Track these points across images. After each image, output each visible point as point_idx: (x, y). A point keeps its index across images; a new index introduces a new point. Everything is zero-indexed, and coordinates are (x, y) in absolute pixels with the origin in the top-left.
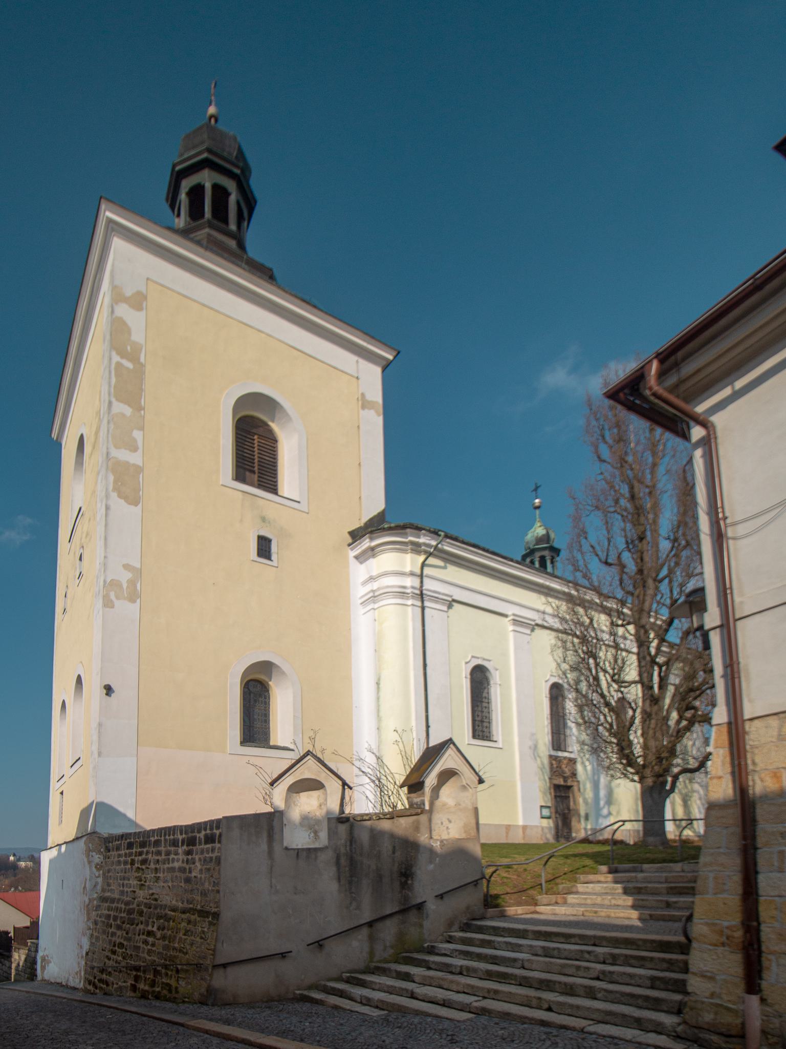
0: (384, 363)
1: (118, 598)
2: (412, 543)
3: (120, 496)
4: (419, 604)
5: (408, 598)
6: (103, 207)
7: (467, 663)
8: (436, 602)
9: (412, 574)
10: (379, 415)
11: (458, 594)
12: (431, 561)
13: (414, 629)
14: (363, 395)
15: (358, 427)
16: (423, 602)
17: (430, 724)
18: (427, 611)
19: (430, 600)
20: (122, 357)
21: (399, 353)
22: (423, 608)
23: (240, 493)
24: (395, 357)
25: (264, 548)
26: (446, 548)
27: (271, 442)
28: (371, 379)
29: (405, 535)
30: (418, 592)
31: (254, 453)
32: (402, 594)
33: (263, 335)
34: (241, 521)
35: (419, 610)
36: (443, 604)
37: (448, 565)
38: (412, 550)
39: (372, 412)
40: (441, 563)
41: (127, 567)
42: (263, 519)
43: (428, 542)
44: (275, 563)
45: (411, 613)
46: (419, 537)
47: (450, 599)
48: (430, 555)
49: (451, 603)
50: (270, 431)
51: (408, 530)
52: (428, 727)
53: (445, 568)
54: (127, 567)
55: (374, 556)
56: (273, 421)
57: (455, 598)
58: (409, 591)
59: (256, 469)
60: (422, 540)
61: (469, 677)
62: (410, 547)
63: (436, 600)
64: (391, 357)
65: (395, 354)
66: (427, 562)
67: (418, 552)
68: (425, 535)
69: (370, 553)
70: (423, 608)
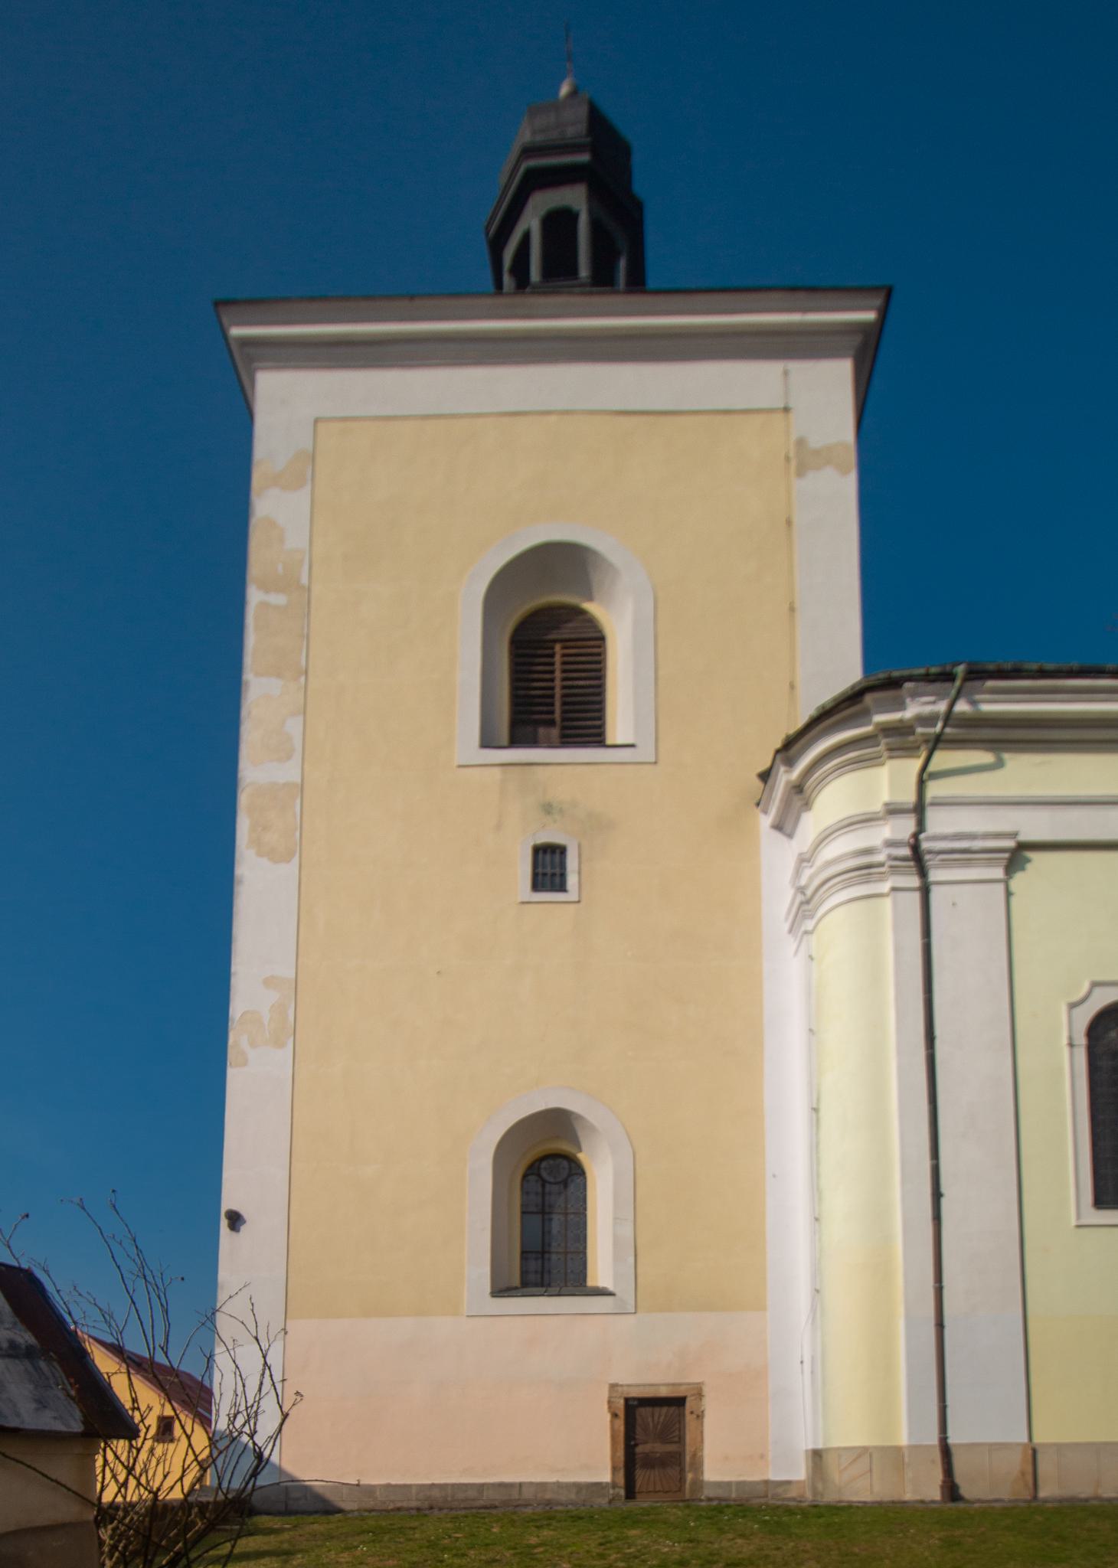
0: (857, 340)
1: (253, 1044)
2: (888, 730)
3: (260, 854)
4: (914, 881)
5: (882, 878)
6: (225, 320)
7: (1073, 1006)
8: (967, 863)
9: (893, 810)
10: (845, 472)
11: (1035, 826)
12: (943, 759)
13: (898, 950)
14: (801, 443)
15: (789, 523)
16: (923, 873)
17: (944, 1189)
18: (936, 894)
19: (945, 864)
20: (267, 591)
21: (889, 292)
22: (925, 891)
23: (497, 771)
24: (884, 313)
25: (548, 868)
26: (986, 708)
27: (588, 650)
28: (822, 396)
29: (865, 715)
30: (906, 852)
31: (547, 675)
32: (865, 870)
33: (553, 418)
34: (499, 827)
35: (916, 897)
36: (990, 863)
37: (1006, 756)
38: (890, 750)
39: (829, 474)
40: (985, 757)
41: (269, 982)
42: (548, 809)
43: (927, 709)
44: (572, 894)
45: (891, 911)
46: (901, 706)
47: (1010, 844)
48: (937, 742)
49: (1017, 856)
50: (591, 622)
51: (869, 699)
52: (937, 1195)
53: (999, 764)
54: (269, 982)
55: (807, 805)
56: (590, 599)
57: (1026, 836)
58: (881, 857)
59: (557, 716)
60: (912, 710)
61: (1082, 1040)
62: (884, 741)
63: (966, 856)
64: (870, 316)
65: (878, 302)
66: (931, 768)
67: (909, 751)
68: (914, 695)
69: (797, 802)
70: (925, 891)
